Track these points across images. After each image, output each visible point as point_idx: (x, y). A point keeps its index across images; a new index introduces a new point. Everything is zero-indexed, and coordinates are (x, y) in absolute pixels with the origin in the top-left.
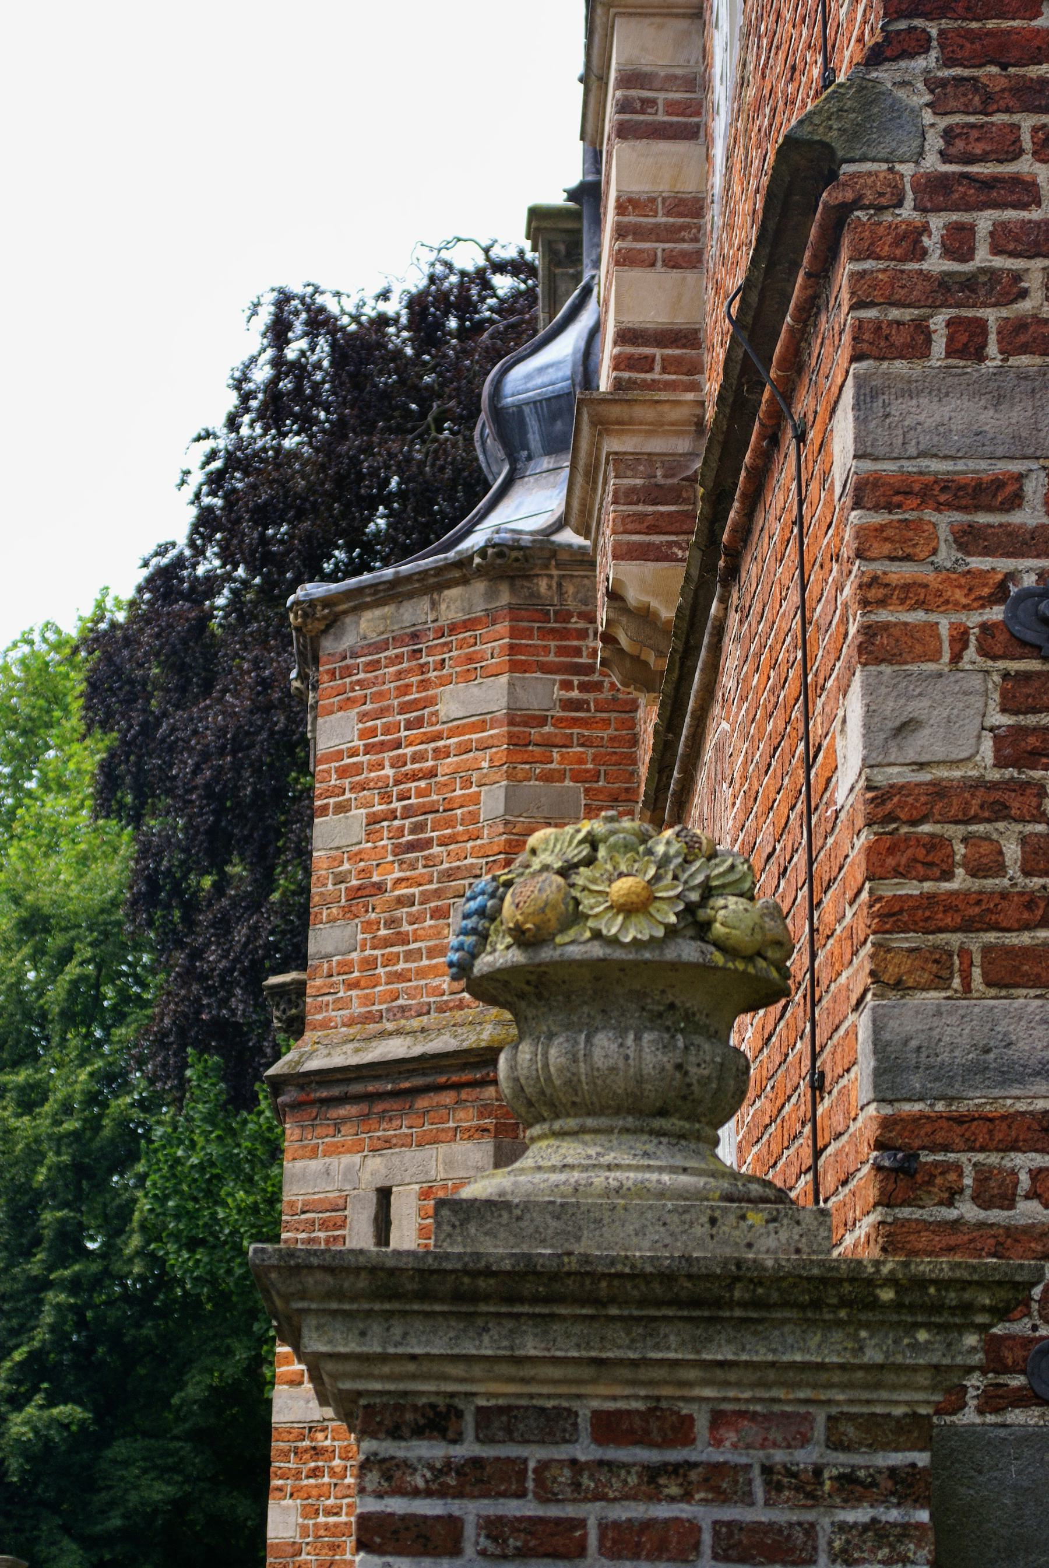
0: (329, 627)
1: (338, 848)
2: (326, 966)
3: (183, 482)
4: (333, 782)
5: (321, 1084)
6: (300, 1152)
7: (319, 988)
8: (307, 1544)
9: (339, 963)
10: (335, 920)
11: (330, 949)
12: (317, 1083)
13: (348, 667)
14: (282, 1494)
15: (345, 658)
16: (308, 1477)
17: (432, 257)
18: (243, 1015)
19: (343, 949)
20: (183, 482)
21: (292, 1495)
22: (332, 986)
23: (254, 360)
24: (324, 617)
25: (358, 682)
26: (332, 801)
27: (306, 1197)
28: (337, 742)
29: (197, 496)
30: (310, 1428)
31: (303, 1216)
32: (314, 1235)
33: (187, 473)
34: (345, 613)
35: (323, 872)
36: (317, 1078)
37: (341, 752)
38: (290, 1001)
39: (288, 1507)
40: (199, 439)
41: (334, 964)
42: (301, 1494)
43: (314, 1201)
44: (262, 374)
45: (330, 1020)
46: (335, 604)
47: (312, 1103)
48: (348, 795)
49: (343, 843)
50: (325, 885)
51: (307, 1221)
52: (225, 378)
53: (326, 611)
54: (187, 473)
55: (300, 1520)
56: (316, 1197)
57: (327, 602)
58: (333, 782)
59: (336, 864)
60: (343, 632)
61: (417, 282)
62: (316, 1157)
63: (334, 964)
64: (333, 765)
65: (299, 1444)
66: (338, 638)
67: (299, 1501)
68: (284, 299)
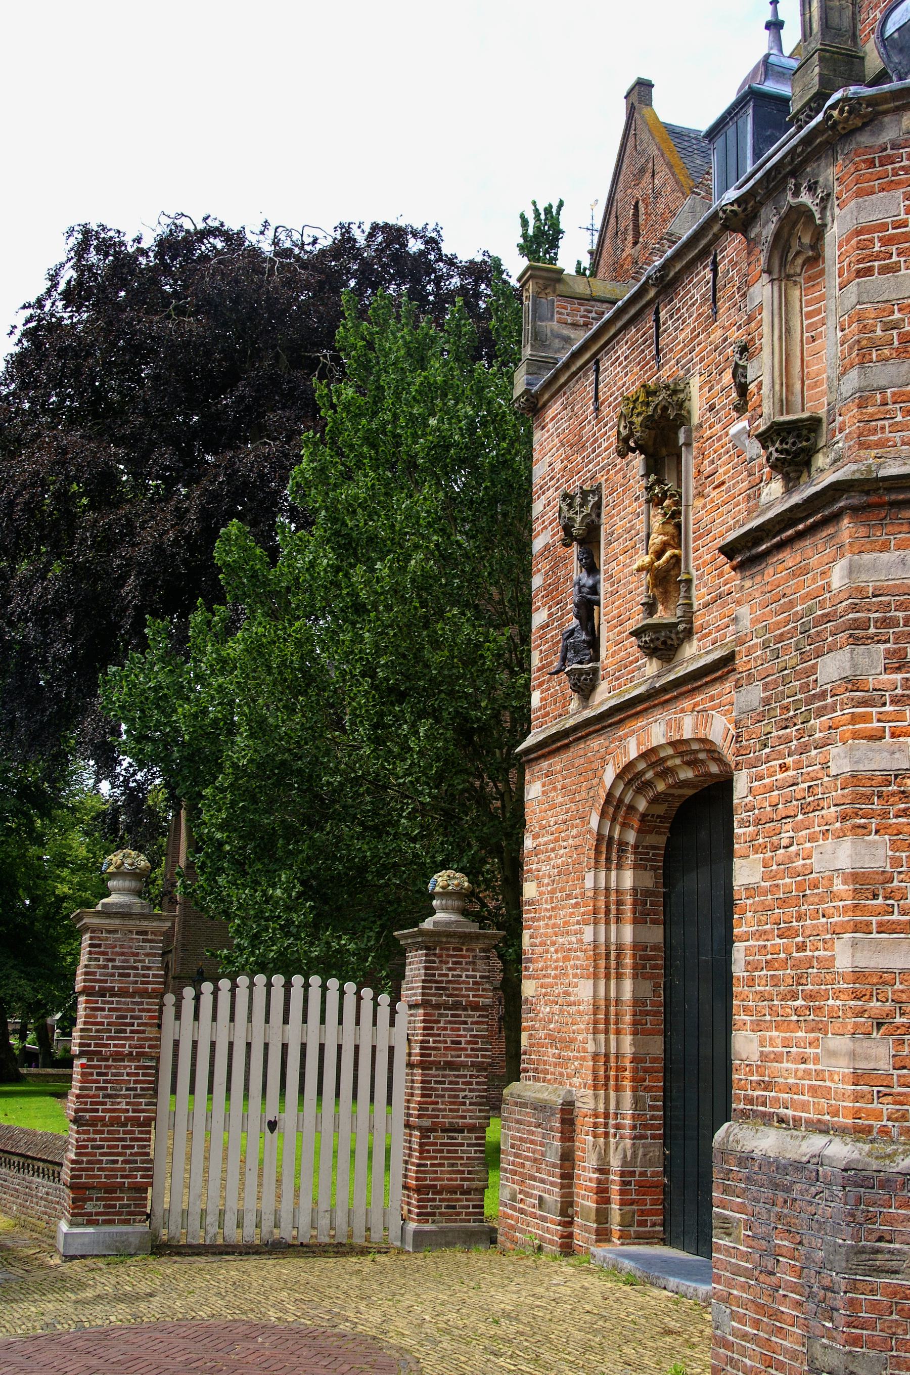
0: (865, 125)
1: (887, 301)
2: (878, 396)
3: (12, 333)
4: (877, 249)
5: (889, 490)
6: (868, 546)
7: (872, 415)
8: (900, 873)
9: (894, 394)
10: (887, 359)
11: (883, 383)
12: (885, 489)
13: (889, 156)
14: (865, 831)
15: (885, 149)
16: (897, 816)
17: (169, 221)
18: (34, 639)
19: (899, 383)
20: (12, 333)
21: (877, 832)
22: (887, 412)
23: (62, 265)
24: (865, 116)
25: (902, 168)
26: (876, 264)
27: (878, 584)
28: (880, 216)
29: (20, 341)
30: (896, 776)
31: (874, 599)
32: (888, 615)
33: (15, 327)
34: (885, 113)
35: (871, 321)
36: (887, 484)
37: (886, 224)
38: (799, 436)
39: (875, 842)
40: (24, 307)
41: (889, 394)
42: (889, 831)
43: (888, 586)
44: (69, 274)
45: (888, 440)
46: (877, 104)
47: (880, 506)
48: (895, 258)
49: (894, 296)
50: (874, 331)
51: (880, 603)
52: (44, 274)
53: (870, 109)
54: (15, 327)
55: (890, 853)
56: (890, 583)
57: (871, 101)
58: (877, 249)
59: (885, 314)
60: (881, 128)
61: (162, 230)
62: (889, 550)
63: (889, 394)
64: (876, 235)
65: (884, 789)
66: (876, 133)
67: (887, 837)
68: (86, 232)
